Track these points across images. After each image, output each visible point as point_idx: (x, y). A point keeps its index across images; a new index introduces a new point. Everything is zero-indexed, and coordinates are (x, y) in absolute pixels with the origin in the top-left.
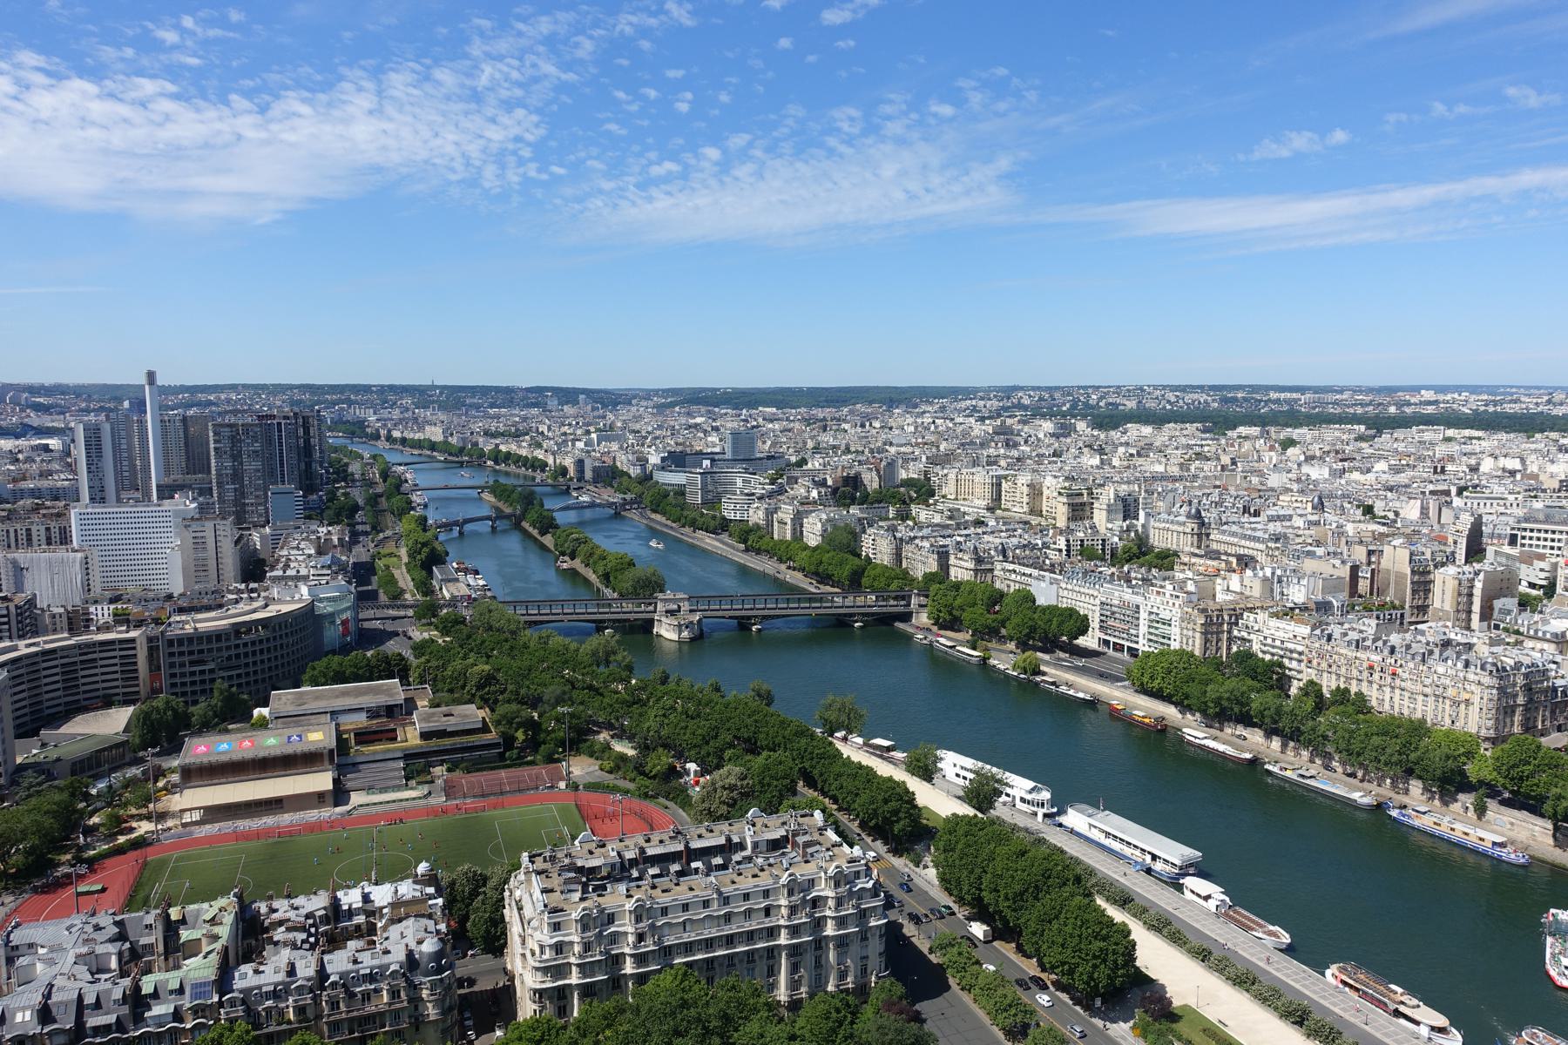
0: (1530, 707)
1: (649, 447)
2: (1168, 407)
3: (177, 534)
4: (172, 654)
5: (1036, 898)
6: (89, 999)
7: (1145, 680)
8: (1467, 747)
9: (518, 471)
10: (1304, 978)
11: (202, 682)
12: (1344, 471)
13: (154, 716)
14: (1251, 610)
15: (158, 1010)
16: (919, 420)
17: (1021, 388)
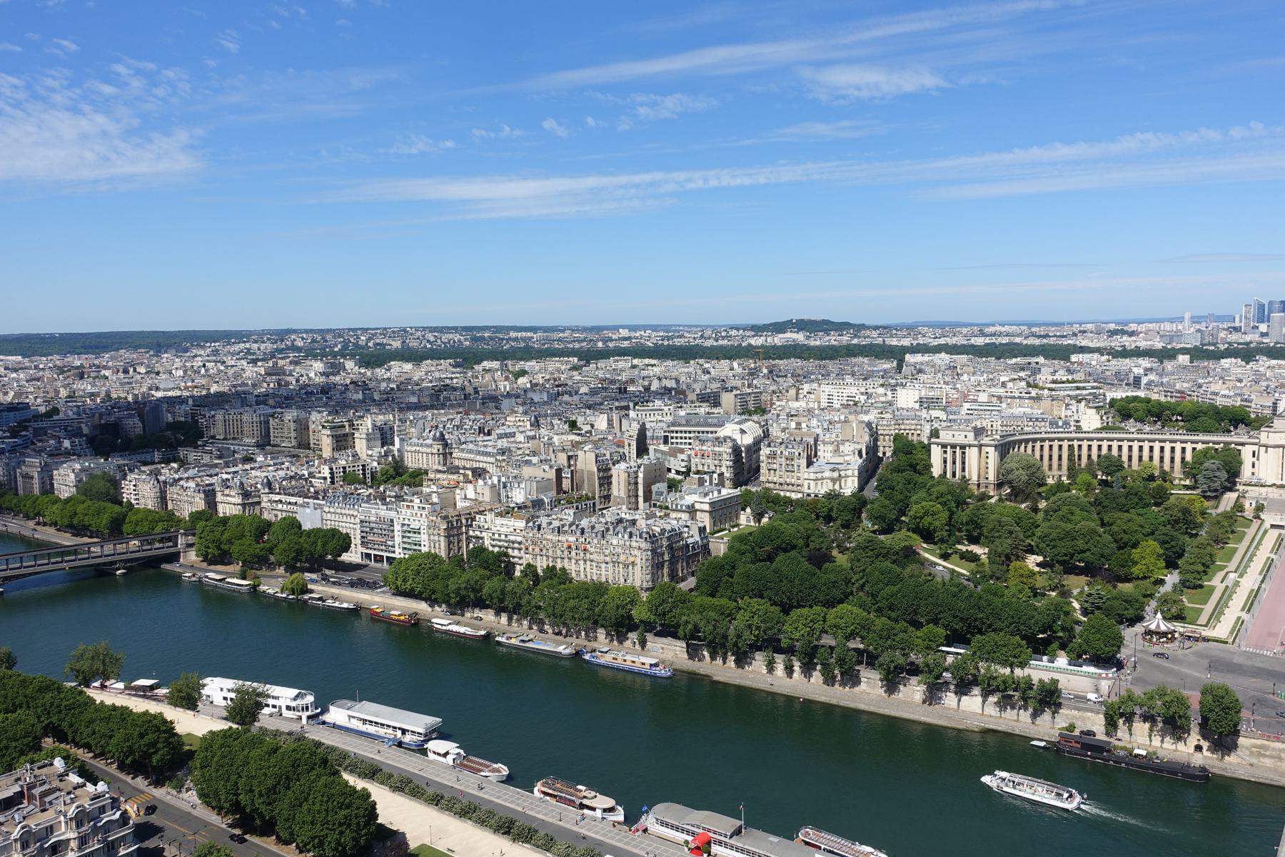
0: (673, 562)
2: (429, 346)
5: (288, 788)
7: (399, 583)
8: (631, 596)
10: (616, 834)
12: (558, 394)
14: (481, 513)
16: (188, 364)
17: (295, 331)
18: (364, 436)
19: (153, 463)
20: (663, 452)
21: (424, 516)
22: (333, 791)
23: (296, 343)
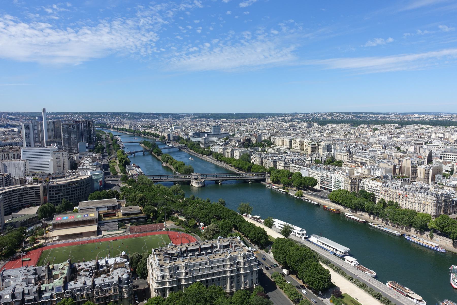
0: (446, 206)
1: (189, 130)
2: (341, 119)
3: (52, 156)
4: (50, 191)
5: (302, 262)
6: (26, 292)
7: (334, 198)
8: (428, 218)
9: (151, 137)
11: (59, 199)
12: (392, 137)
13: (45, 209)
14: (365, 178)
15: (46, 295)
16: (268, 123)
17: (298, 113)
19: (259, 151)
20: (440, 162)
22: (317, 267)
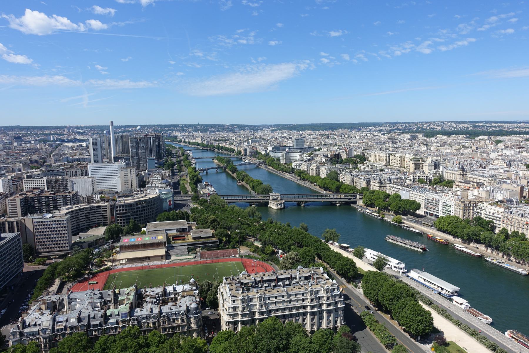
1: (268, 144)
2: (453, 129)
5: (397, 301)
6: (92, 316)
7: (441, 226)
14: (481, 202)
15: (112, 320)
17: (399, 123)
18: (428, 165)
19: (349, 169)
21: (453, 200)
22: (415, 308)
23: (399, 127)
